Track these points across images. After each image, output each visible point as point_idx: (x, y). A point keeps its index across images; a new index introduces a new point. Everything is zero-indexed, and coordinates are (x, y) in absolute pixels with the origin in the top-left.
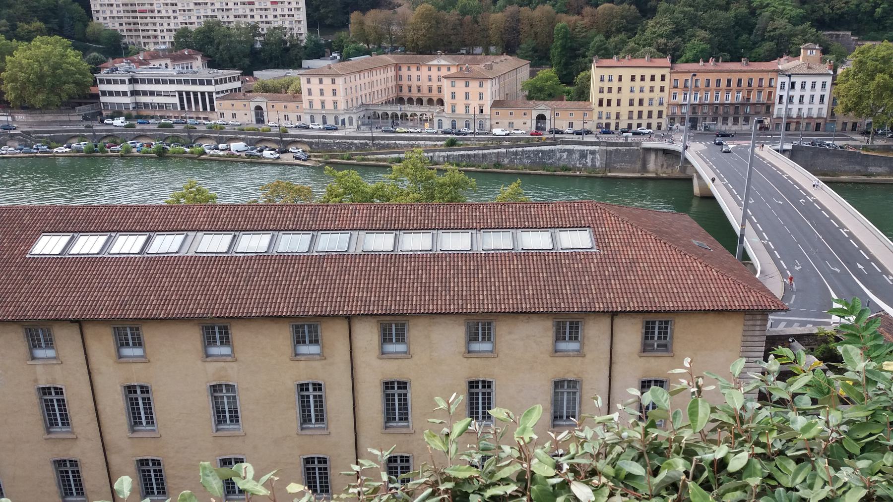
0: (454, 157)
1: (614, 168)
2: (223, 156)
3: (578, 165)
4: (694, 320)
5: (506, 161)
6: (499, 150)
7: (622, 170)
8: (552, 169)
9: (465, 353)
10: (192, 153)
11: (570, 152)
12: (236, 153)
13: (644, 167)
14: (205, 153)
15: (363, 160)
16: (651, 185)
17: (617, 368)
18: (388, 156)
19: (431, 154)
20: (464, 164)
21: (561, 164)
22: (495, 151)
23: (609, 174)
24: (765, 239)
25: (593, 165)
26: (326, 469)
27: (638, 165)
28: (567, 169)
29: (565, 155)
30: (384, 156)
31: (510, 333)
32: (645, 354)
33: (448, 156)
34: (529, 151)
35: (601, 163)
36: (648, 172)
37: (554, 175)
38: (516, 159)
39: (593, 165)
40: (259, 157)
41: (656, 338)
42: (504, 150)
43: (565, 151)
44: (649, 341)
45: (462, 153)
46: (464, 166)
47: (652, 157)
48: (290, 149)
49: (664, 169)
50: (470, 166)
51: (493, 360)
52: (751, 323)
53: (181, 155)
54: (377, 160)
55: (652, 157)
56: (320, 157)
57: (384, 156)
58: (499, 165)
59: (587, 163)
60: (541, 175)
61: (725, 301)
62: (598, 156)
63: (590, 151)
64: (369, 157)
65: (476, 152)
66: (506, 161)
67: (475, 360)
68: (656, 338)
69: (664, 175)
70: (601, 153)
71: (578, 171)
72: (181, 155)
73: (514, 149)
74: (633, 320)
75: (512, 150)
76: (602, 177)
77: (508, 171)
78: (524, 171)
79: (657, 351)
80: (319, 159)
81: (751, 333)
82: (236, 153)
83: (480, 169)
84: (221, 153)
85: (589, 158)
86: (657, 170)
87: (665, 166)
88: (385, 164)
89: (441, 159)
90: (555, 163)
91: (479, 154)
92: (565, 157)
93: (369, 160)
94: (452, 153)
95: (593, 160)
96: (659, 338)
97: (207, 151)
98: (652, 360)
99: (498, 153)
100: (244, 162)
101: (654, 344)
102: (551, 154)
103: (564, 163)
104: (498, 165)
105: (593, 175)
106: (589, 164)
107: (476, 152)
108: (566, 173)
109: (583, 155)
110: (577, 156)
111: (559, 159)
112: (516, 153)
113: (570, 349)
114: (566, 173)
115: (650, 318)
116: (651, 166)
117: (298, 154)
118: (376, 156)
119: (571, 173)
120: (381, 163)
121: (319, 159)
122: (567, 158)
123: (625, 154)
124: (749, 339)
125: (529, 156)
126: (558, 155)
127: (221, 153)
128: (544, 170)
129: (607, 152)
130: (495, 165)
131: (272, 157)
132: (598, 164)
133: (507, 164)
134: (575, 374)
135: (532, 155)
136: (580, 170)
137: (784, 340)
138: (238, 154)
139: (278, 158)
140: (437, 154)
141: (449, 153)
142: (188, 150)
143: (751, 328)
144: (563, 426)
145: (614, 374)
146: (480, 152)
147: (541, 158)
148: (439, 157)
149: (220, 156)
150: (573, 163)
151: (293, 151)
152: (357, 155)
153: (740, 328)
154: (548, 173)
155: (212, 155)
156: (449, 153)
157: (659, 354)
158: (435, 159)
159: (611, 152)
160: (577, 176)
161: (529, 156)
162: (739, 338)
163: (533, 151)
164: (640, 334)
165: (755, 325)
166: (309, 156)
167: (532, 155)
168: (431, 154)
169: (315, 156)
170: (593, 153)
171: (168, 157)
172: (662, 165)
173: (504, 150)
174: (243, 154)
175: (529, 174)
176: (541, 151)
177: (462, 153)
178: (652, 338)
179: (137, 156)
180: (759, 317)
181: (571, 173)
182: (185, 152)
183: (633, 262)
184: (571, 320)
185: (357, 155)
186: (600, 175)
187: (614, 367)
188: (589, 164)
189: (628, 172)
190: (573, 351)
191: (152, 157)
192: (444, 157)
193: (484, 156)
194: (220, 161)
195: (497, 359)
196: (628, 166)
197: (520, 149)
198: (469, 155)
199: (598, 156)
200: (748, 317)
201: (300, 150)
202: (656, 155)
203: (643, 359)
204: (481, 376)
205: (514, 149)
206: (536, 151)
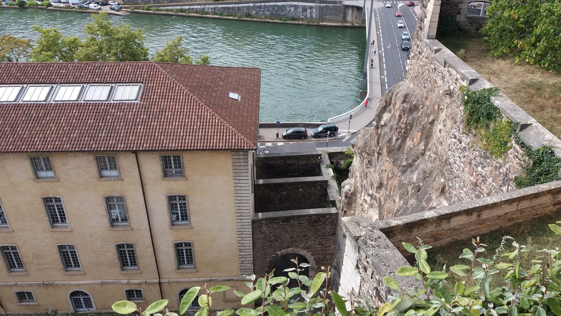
0: (219, 9)
1: (325, 19)
2: (63, 7)
3: (301, 17)
4: (197, 155)
5: (254, 12)
6: (249, 5)
7: (330, 21)
8: (284, 19)
9: (34, 179)
10: (42, 5)
11: (296, 7)
12: (71, 5)
13: (344, 19)
14: (51, 5)
15: (158, 10)
16: (349, 31)
17: (148, 189)
18: (174, 8)
19: (203, 7)
20: (225, 14)
21: (291, 15)
22: (246, 5)
23: (321, 23)
24: (383, 75)
25: (311, 17)
26: (185, 204)
27: (341, 18)
28: (294, 19)
29: (293, 9)
30: (171, 8)
31: (64, 165)
32: (165, 179)
33: (215, 8)
34: (268, 6)
35: (316, 15)
36: (347, 22)
37: (285, 23)
38: (260, 11)
39: (311, 17)
40: (87, 8)
41: (173, 167)
42: (252, 5)
43: (293, 6)
44: (169, 169)
45: (224, 6)
46: (225, 16)
47: (350, 12)
48: (109, 3)
49: (358, 20)
50: (228, 16)
51: (57, 184)
52: (236, 157)
53: (35, 7)
54: (167, 10)
55: (350, 12)
56: (129, 8)
57: (171, 8)
58: (249, 15)
59: (307, 15)
60: (276, 23)
61: (215, 142)
62: (314, 11)
63: (309, 6)
64: (161, 8)
65: (233, 5)
66: (254, 12)
67: (44, 183)
68: (173, 167)
69: (357, 25)
70: (316, 7)
71: (301, 20)
72: (35, 7)
73: (259, 4)
74: (152, 156)
75: (257, 4)
76: (316, 26)
77: (255, 19)
78: (266, 20)
79: (176, 176)
80: (128, 10)
81: (238, 164)
82: (71, 5)
83: (236, 18)
84: (62, 5)
85: (309, 11)
86: (353, 20)
87: (358, 18)
88: (172, 13)
89: (210, 10)
90: (286, 14)
91: (235, 7)
92: (293, 10)
93: (161, 10)
94: (217, 6)
95: (311, 13)
96: (176, 167)
97: (53, 4)
98: (173, 182)
99: (248, 6)
100: (77, 12)
101: (173, 171)
102: (283, 8)
103: (292, 15)
104: (248, 15)
105: (310, 23)
106: (309, 16)
107: (233, 5)
108: (293, 22)
109: (305, 9)
110: (300, 10)
111: (289, 12)
112: (260, 7)
113: (112, 175)
114: (293, 22)
115: (166, 154)
116: (349, 18)
117: (114, 6)
118: (166, 8)
119: (296, 22)
120: (170, 13)
121: (128, 10)
122: (294, 11)
123: (332, 9)
124: (237, 168)
125: (269, 9)
126: (288, 9)
127: (62, 5)
128: (279, 19)
129: (320, 7)
130: (246, 15)
131: (95, 8)
132: (314, 16)
133: (255, 14)
134: (118, 192)
135: (271, 9)
136: (302, 20)
137: (316, 158)
138: (73, 6)
139: (100, 9)
140: (207, 6)
141: (215, 6)
142: (39, 3)
143: (237, 161)
144: (120, 226)
145: (146, 192)
146: (236, 5)
147: (277, 11)
148: (208, 8)
149: (61, 8)
150: (298, 15)
151: (111, 4)
152: (153, 6)
153: (230, 161)
154: (281, 22)
155: (55, 7)
156: (215, 6)
157: (176, 178)
158: (206, 10)
159: (323, 7)
160: (300, 25)
161: (269, 9)
162: (231, 168)
163: (272, 6)
164: (160, 165)
165: (240, 159)
166: (122, 8)
167: (271, 9)
168: (203, 7)
169: (125, 8)
170: (311, 8)
171: (26, 8)
172: (356, 18)
173: (252, 5)
174: (76, 6)
175: (269, 22)
176: (277, 6)
177: (224, 6)
178: (171, 167)
179: (5, 8)
180: (241, 153)
181: (296, 22)
182: (38, 5)
183: (162, 111)
184: (108, 155)
185: (153, 6)
186: (315, 24)
187: (145, 187)
188: (309, 16)
189: (334, 22)
190: (115, 176)
191: (15, 8)
192: (212, 9)
193: (239, 8)
194: (60, 11)
195: (59, 183)
196: (334, 18)
197: (263, 4)
198: (228, 8)
199: (314, 11)
200: (233, 153)
201: (116, 3)
202: (353, 10)
203: (165, 182)
204: (51, 194)
205: (259, 4)
206: (274, 5)
